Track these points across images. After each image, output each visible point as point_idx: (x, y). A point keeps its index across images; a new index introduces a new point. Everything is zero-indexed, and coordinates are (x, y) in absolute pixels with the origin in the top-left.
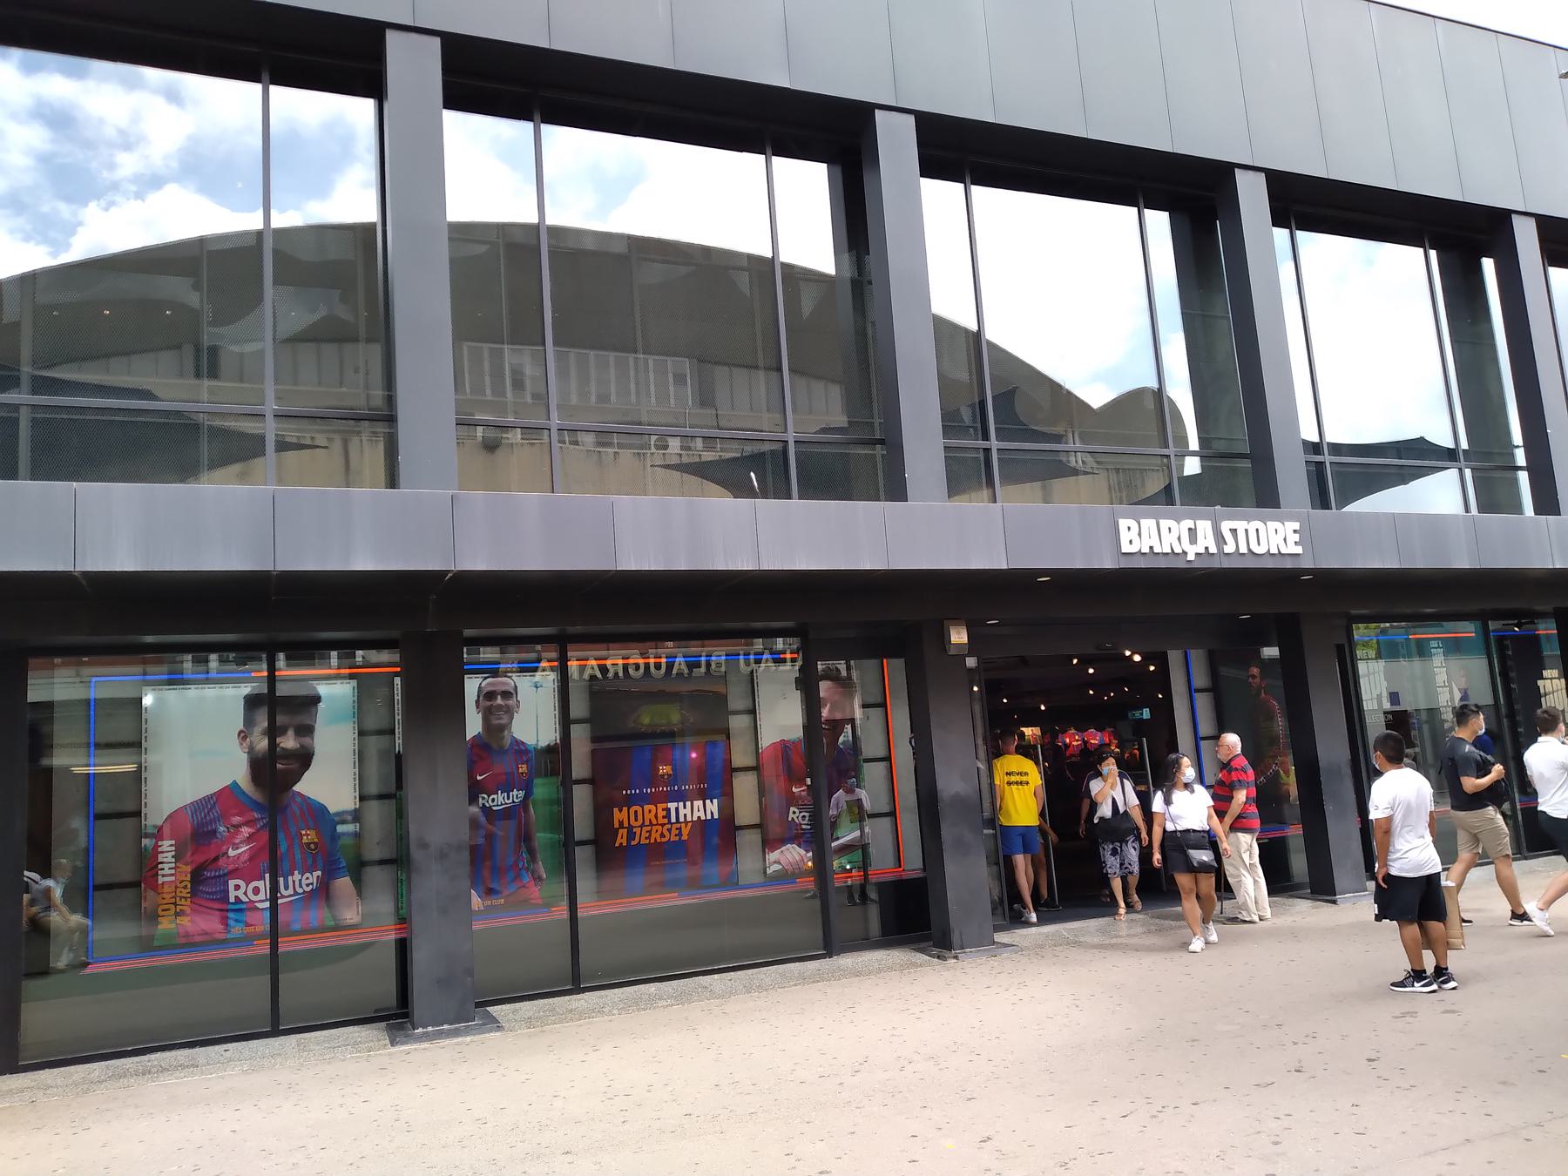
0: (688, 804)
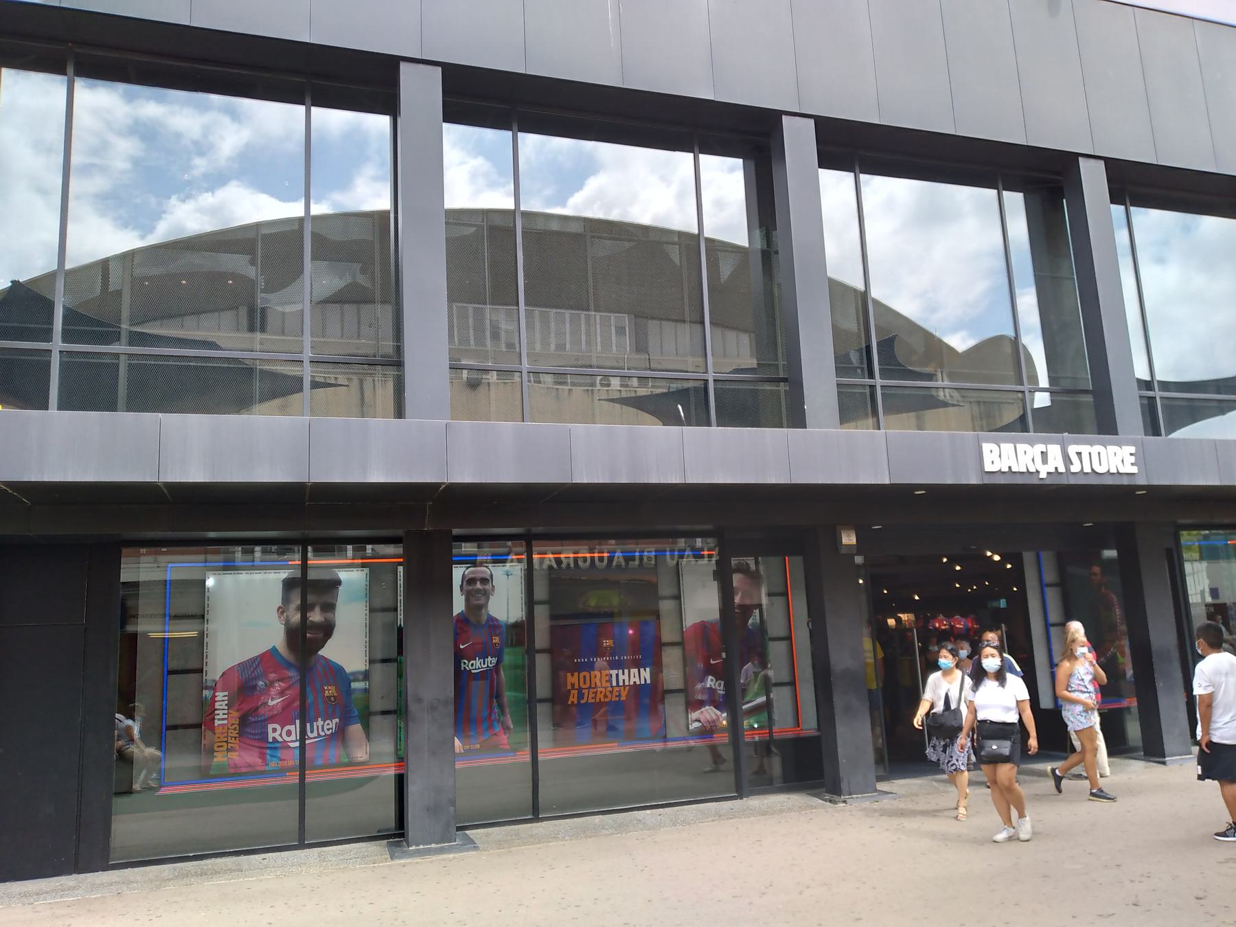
0: (626, 671)
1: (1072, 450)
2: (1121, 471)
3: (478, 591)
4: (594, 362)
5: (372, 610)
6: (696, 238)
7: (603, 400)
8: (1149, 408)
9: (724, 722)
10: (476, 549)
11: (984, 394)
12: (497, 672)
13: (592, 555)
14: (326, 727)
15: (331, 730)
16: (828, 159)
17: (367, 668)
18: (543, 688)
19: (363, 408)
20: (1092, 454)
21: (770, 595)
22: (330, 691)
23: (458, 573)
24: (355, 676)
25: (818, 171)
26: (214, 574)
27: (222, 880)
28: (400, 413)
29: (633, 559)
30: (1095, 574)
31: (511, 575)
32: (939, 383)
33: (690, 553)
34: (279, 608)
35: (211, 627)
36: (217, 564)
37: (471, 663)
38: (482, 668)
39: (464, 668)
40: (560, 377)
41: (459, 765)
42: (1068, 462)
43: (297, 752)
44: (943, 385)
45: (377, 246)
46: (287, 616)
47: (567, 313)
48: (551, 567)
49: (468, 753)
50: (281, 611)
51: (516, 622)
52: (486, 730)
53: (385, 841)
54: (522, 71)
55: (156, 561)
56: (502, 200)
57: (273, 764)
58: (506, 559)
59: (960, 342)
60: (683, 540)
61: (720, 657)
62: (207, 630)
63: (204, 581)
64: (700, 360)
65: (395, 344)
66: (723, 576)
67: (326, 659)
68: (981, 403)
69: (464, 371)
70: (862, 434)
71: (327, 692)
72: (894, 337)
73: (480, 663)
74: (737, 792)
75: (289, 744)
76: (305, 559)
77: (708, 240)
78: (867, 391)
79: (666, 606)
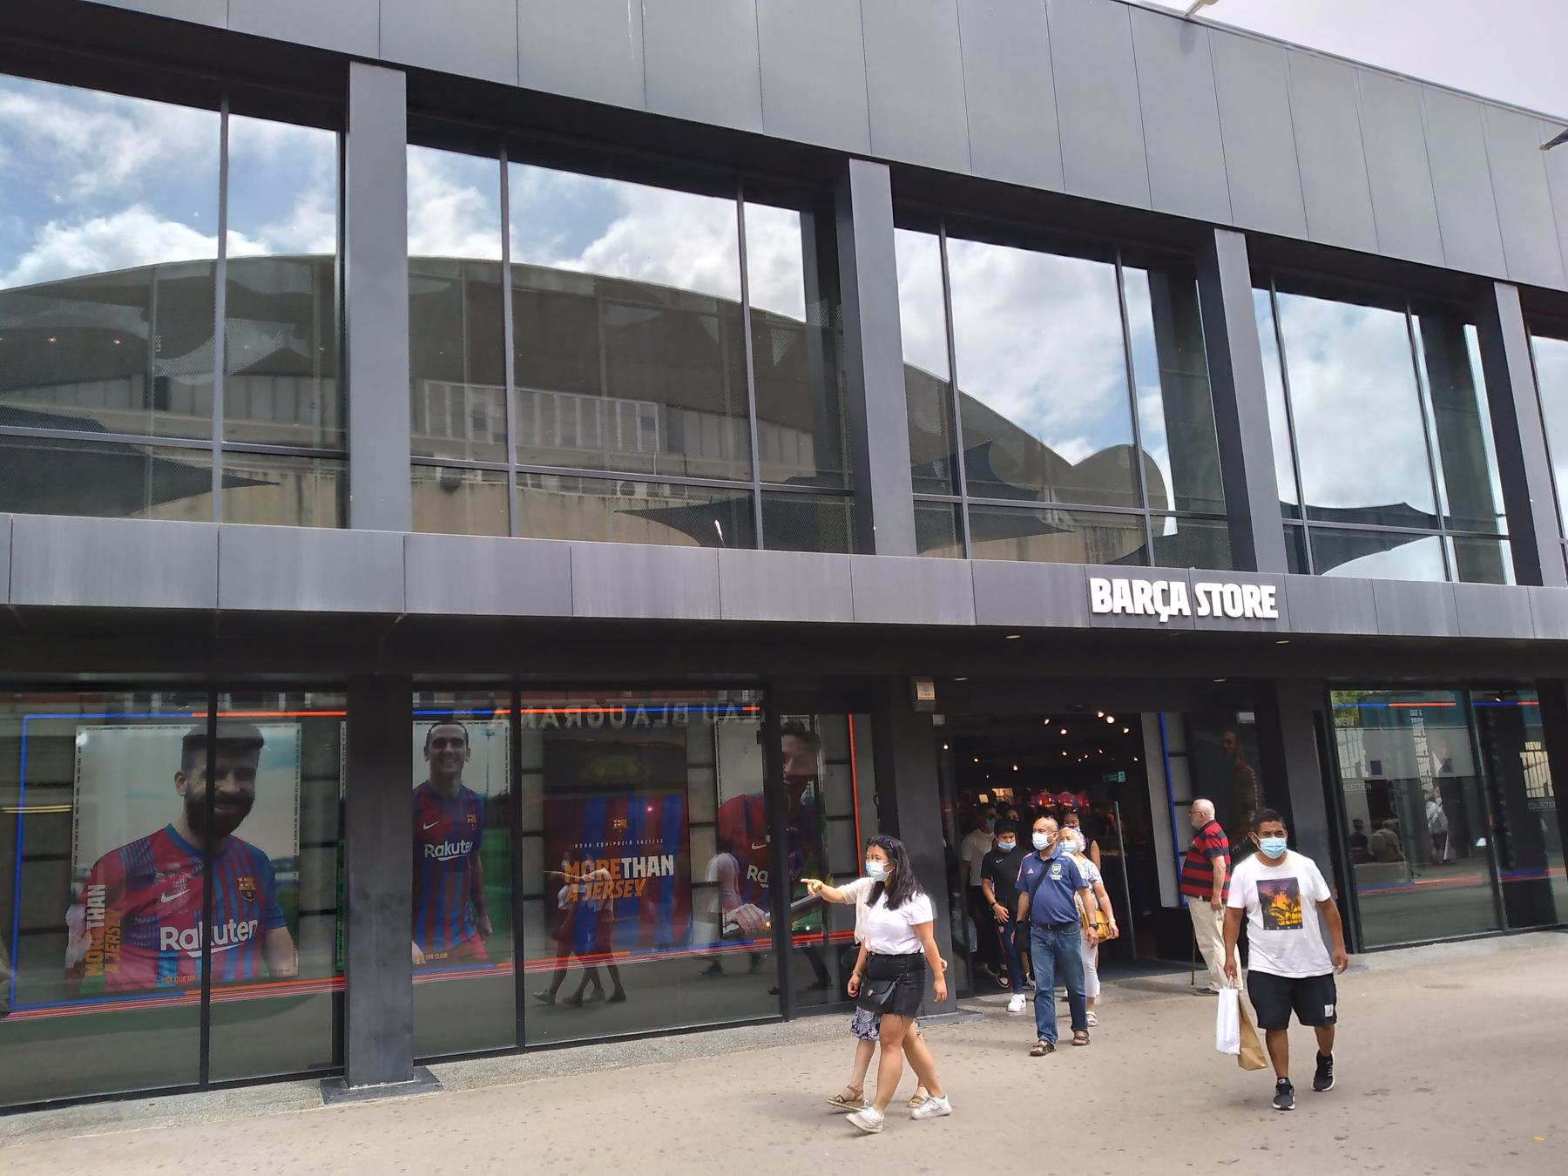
0: (643, 859)
1: (1200, 588)
2: (1258, 615)
3: (450, 754)
4: (608, 463)
5: (306, 778)
6: (740, 307)
7: (623, 511)
8: (1295, 539)
9: (768, 924)
10: (453, 702)
11: (1100, 518)
12: (474, 862)
13: (606, 710)
14: (239, 931)
15: (246, 936)
16: (905, 219)
17: (298, 854)
18: (531, 881)
19: (301, 515)
20: (1224, 594)
21: (828, 762)
22: (246, 883)
23: (421, 733)
24: (281, 865)
25: (893, 234)
26: (88, 729)
27: (91, 1133)
28: (343, 521)
29: (659, 715)
30: (1229, 742)
31: (493, 734)
32: (1046, 504)
33: (733, 709)
34: (177, 775)
35: (83, 799)
36: (98, 716)
37: (438, 848)
38: (453, 855)
39: (429, 854)
40: (568, 482)
41: (416, 981)
42: (1195, 602)
43: (199, 963)
44: (1051, 505)
45: (317, 302)
46: (189, 785)
47: (578, 398)
48: (550, 726)
49: (430, 966)
50: (180, 778)
51: (499, 795)
52: (457, 935)
53: (318, 1080)
54: (513, 83)
55: (12, 712)
56: (486, 248)
57: (169, 979)
58: (493, 714)
59: (1073, 452)
60: (726, 692)
61: (763, 841)
62: (77, 803)
63: (74, 739)
64: (745, 464)
65: (339, 430)
66: (769, 739)
67: (241, 842)
68: (1098, 529)
69: (437, 468)
70: (943, 563)
71: (242, 885)
72: (987, 446)
73: (451, 849)
74: (781, 1013)
75: (189, 953)
76: (213, 710)
77: (753, 311)
78: (952, 510)
79: (697, 777)
